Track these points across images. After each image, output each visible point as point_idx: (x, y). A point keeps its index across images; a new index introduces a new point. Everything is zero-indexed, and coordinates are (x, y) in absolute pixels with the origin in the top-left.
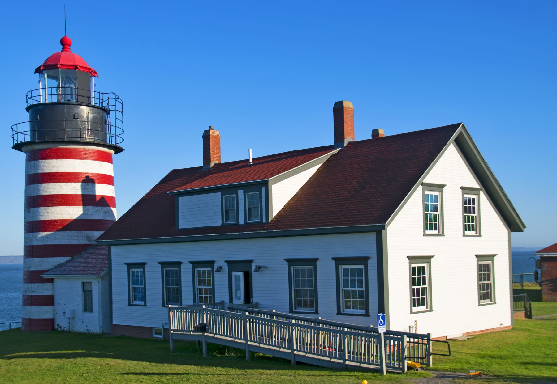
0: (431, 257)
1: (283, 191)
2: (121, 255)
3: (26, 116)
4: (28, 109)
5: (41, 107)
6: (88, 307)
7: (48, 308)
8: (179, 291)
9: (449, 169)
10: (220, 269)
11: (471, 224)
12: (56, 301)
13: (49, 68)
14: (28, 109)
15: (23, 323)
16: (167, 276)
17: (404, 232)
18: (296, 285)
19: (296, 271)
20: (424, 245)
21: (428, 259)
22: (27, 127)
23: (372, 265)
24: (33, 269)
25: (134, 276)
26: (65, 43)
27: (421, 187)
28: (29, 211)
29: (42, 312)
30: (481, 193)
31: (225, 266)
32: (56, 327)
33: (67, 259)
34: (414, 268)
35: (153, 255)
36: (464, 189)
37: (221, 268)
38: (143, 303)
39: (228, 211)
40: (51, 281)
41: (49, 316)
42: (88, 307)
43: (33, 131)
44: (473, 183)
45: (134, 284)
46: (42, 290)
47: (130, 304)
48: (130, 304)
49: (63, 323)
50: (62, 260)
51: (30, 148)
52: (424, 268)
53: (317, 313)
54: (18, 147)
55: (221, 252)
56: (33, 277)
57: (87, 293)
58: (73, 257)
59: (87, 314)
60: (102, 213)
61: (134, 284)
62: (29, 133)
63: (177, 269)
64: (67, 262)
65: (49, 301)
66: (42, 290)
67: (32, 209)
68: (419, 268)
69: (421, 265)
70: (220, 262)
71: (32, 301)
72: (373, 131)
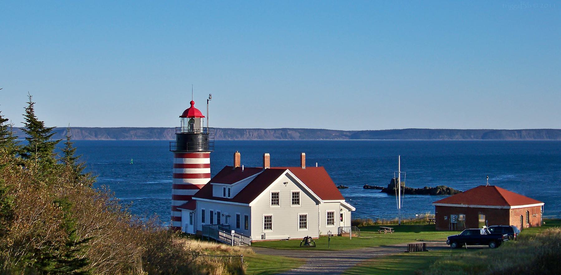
6: (191, 223)
11: (296, 199)
13: (185, 115)
26: (192, 103)
40: (181, 211)
46: (177, 214)
50: (185, 202)
57: (191, 217)
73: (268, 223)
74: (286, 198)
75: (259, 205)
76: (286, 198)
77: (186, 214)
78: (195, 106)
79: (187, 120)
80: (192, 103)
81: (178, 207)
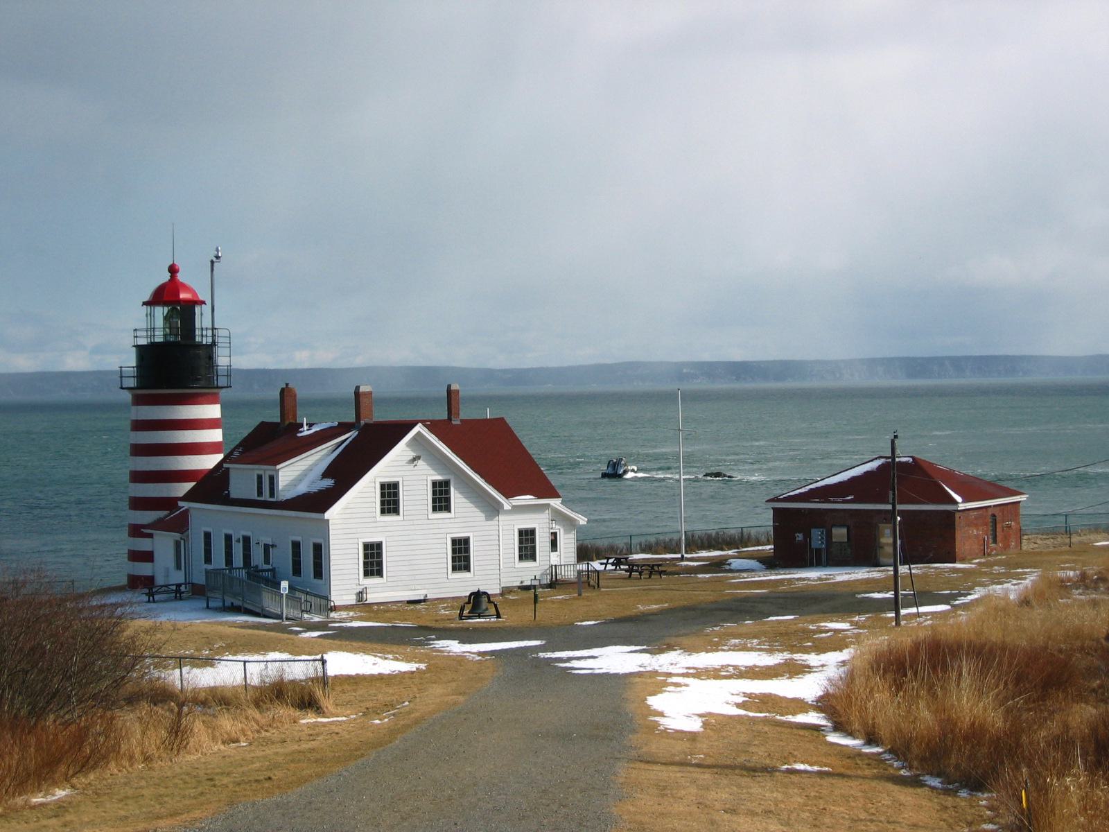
6: (178, 567)
7: (149, 565)
11: (441, 501)
12: (156, 555)
26: (173, 270)
29: (144, 569)
40: (151, 536)
46: (143, 545)
65: (148, 557)
73: (373, 560)
74: (416, 495)
75: (352, 518)
77: (163, 544)
78: (181, 277)
79: (160, 312)
80: (173, 270)
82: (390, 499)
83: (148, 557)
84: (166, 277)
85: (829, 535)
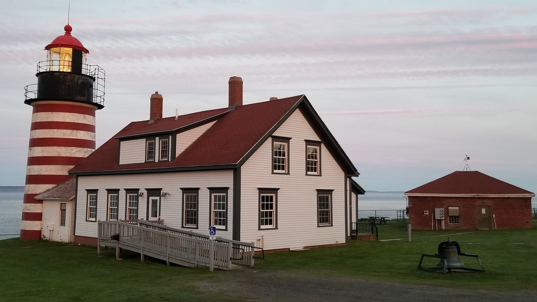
0: (97, 190)
1: (185, 141)
2: (85, 184)
3: (36, 80)
4: (37, 75)
5: (45, 74)
6: (63, 223)
8: (196, 214)
9: (296, 128)
10: (142, 195)
11: (312, 166)
12: (44, 217)
14: (37, 75)
15: (21, 234)
16: (328, 204)
17: (257, 171)
18: (187, 207)
19: (215, 196)
20: (271, 181)
21: (275, 191)
22: (36, 88)
23: (231, 193)
24: (30, 193)
25: (272, 205)
26: (68, 29)
27: (270, 140)
28: (31, 149)
29: (33, 226)
30: (322, 145)
31: (145, 193)
32: (42, 237)
33: (54, 186)
34: (263, 197)
35: (102, 184)
36: (308, 142)
37: (143, 194)
38: (94, 219)
39: (150, 153)
41: (38, 229)
42: (63, 223)
43: (39, 91)
44: (315, 137)
45: (111, 206)
46: (35, 208)
47: (86, 221)
48: (86, 221)
49: (46, 234)
50: (50, 186)
51: (35, 103)
52: (272, 197)
53: (197, 228)
54: (28, 102)
55: (143, 183)
56: (30, 199)
57: (63, 211)
58: (58, 185)
59: (62, 227)
60: (83, 153)
61: (111, 206)
62: (36, 92)
63: (196, 194)
64: (53, 188)
65: (38, 217)
66: (35, 208)
67: (32, 148)
68: (267, 197)
69: (269, 195)
70: (142, 191)
71: (28, 216)
72: (94, 127)
74: (297, 157)
76: (297, 157)
80: (68, 29)
81: (36, 195)
82: (279, 163)
83: (38, 217)
84: (63, 33)
85: (447, 211)
